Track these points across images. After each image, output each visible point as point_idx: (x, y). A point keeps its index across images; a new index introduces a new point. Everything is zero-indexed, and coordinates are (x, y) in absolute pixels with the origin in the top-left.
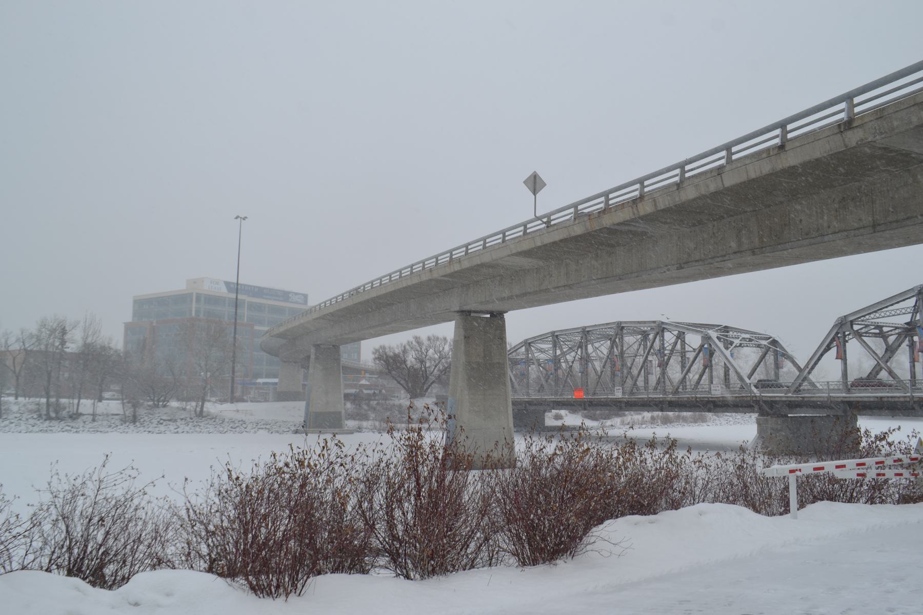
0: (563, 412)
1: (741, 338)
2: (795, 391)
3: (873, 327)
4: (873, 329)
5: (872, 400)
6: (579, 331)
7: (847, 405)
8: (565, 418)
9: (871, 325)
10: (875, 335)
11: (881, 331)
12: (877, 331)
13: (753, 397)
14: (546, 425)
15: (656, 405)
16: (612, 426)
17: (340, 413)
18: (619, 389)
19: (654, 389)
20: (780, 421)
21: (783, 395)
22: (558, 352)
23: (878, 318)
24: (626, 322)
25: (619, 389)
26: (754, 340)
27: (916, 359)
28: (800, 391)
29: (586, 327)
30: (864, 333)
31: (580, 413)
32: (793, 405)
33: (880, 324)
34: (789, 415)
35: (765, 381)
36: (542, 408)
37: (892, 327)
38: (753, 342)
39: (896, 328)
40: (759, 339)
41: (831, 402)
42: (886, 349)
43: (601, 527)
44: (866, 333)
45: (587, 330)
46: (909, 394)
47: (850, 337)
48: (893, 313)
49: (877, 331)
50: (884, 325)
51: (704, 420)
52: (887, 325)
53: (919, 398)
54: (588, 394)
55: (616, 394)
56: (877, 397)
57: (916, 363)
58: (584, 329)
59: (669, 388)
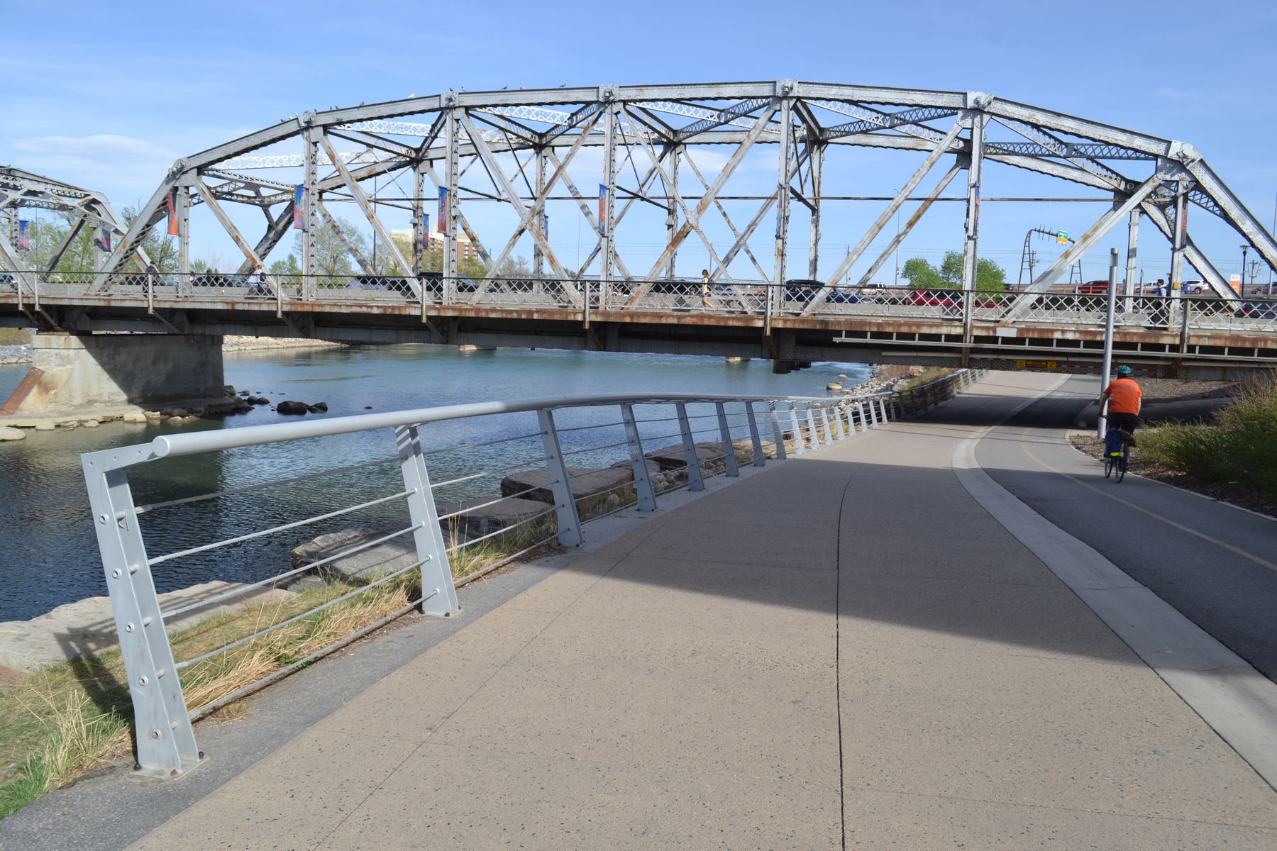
1: (25, 190)
4: (243, 188)
7: (185, 317)
10: (249, 201)
11: (258, 193)
12: (252, 194)
14: (225, 384)
17: (411, 526)
26: (51, 196)
33: (255, 182)
34: (94, 333)
36: (217, 330)
37: (924, 127)
39: (286, 192)
42: (269, 226)
44: (230, 193)
49: (252, 194)
50: (262, 183)
51: (577, 363)
52: (270, 185)
55: (98, 267)
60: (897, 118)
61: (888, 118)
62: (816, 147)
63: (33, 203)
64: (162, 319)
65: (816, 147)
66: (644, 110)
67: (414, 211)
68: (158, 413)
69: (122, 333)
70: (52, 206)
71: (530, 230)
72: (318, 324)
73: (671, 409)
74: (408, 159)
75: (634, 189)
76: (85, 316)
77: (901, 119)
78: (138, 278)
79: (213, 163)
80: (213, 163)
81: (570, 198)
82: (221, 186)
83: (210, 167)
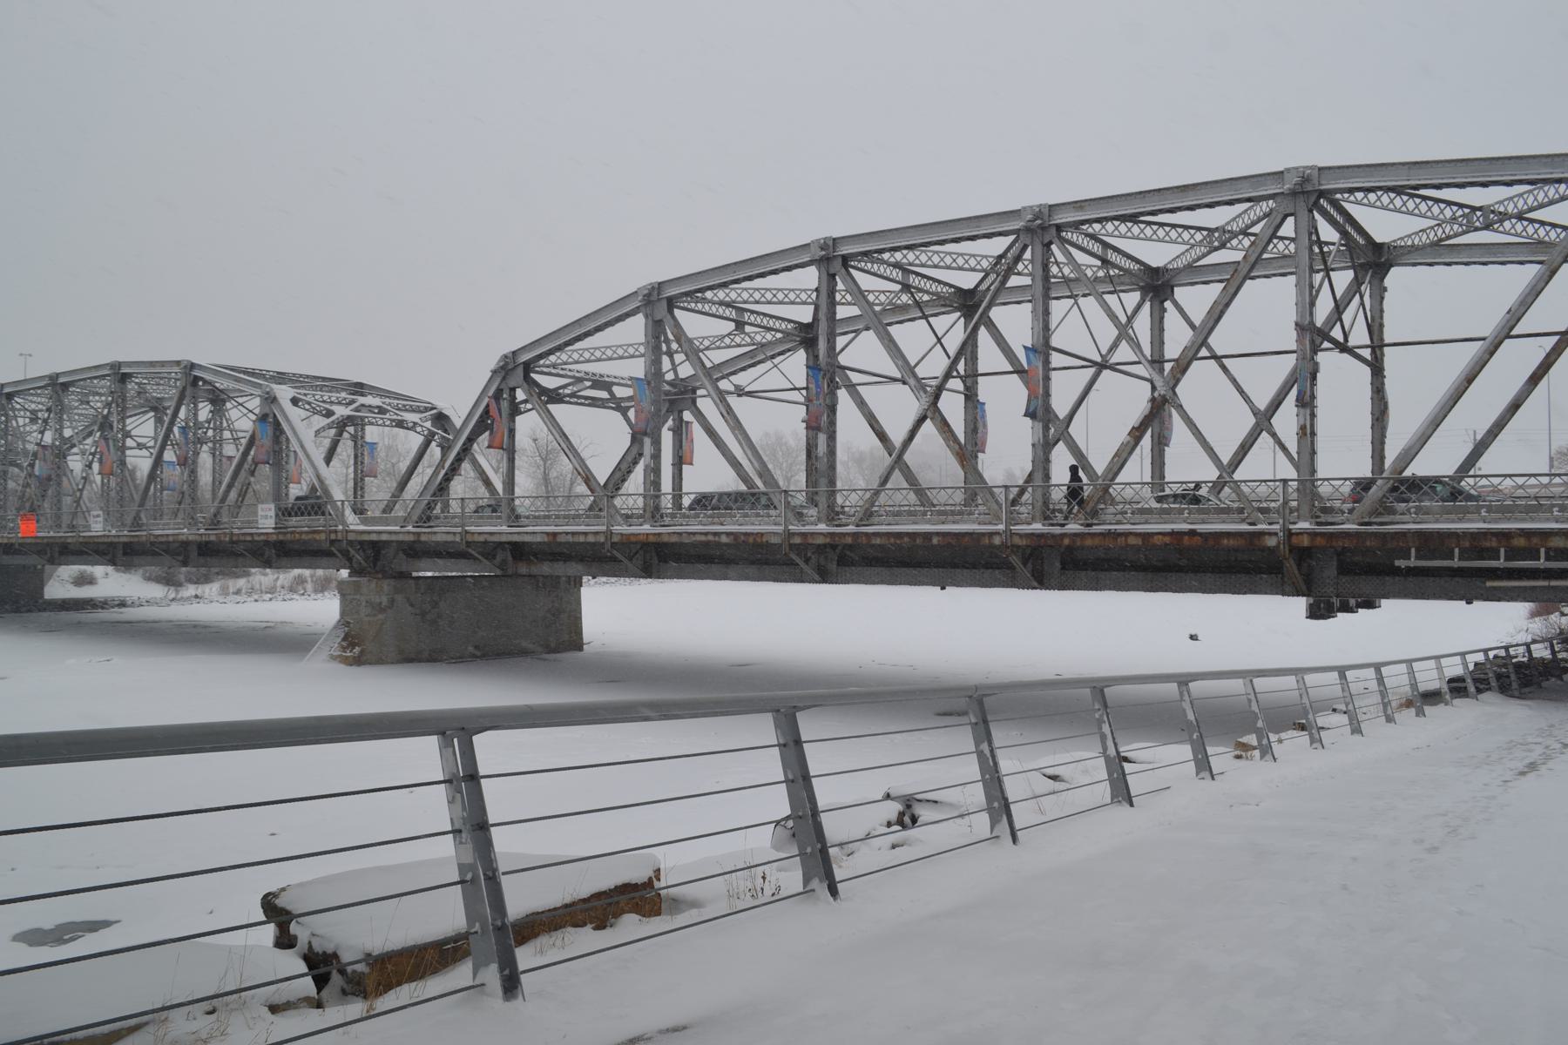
0: (98, 570)
2: (420, 518)
3: (588, 384)
4: (591, 387)
5: (539, 539)
6: (42, 384)
8: (101, 581)
9: (587, 380)
12: (604, 395)
13: (331, 532)
15: (97, 552)
16: (196, 596)
18: (98, 516)
19: (384, 511)
20: (387, 585)
21: (397, 528)
22: (1460, 219)
23: (588, 361)
24: (130, 364)
25: (98, 516)
26: (389, 411)
27: (686, 457)
28: (429, 519)
29: (58, 375)
30: (568, 395)
31: (141, 571)
32: (416, 550)
35: (832, 482)
36: (573, 568)
38: (387, 416)
40: (399, 409)
41: (468, 544)
43: (573, 929)
44: (573, 395)
45: (62, 380)
46: (1001, 527)
47: (529, 406)
48: (587, 355)
49: (604, 395)
50: (614, 380)
53: (622, 534)
54: (193, 522)
56: (547, 534)
57: (684, 466)
58: (116, 366)
59: (849, 501)
60: (1493, 212)
61: (1479, 213)
62: (1151, 295)
63: (380, 422)
64: (480, 557)
65: (1151, 295)
66: (1093, 237)
67: (807, 406)
68: (357, 648)
69: (450, 574)
70: (388, 423)
71: (931, 419)
72: (843, 561)
73: (1432, 663)
74: (779, 335)
75: (1219, 341)
76: (401, 555)
77: (1500, 213)
78: (296, 508)
79: (541, 357)
80: (541, 357)
81: (860, 384)
82: (564, 387)
83: (542, 362)
